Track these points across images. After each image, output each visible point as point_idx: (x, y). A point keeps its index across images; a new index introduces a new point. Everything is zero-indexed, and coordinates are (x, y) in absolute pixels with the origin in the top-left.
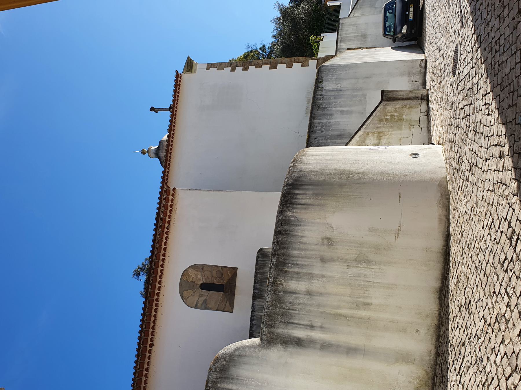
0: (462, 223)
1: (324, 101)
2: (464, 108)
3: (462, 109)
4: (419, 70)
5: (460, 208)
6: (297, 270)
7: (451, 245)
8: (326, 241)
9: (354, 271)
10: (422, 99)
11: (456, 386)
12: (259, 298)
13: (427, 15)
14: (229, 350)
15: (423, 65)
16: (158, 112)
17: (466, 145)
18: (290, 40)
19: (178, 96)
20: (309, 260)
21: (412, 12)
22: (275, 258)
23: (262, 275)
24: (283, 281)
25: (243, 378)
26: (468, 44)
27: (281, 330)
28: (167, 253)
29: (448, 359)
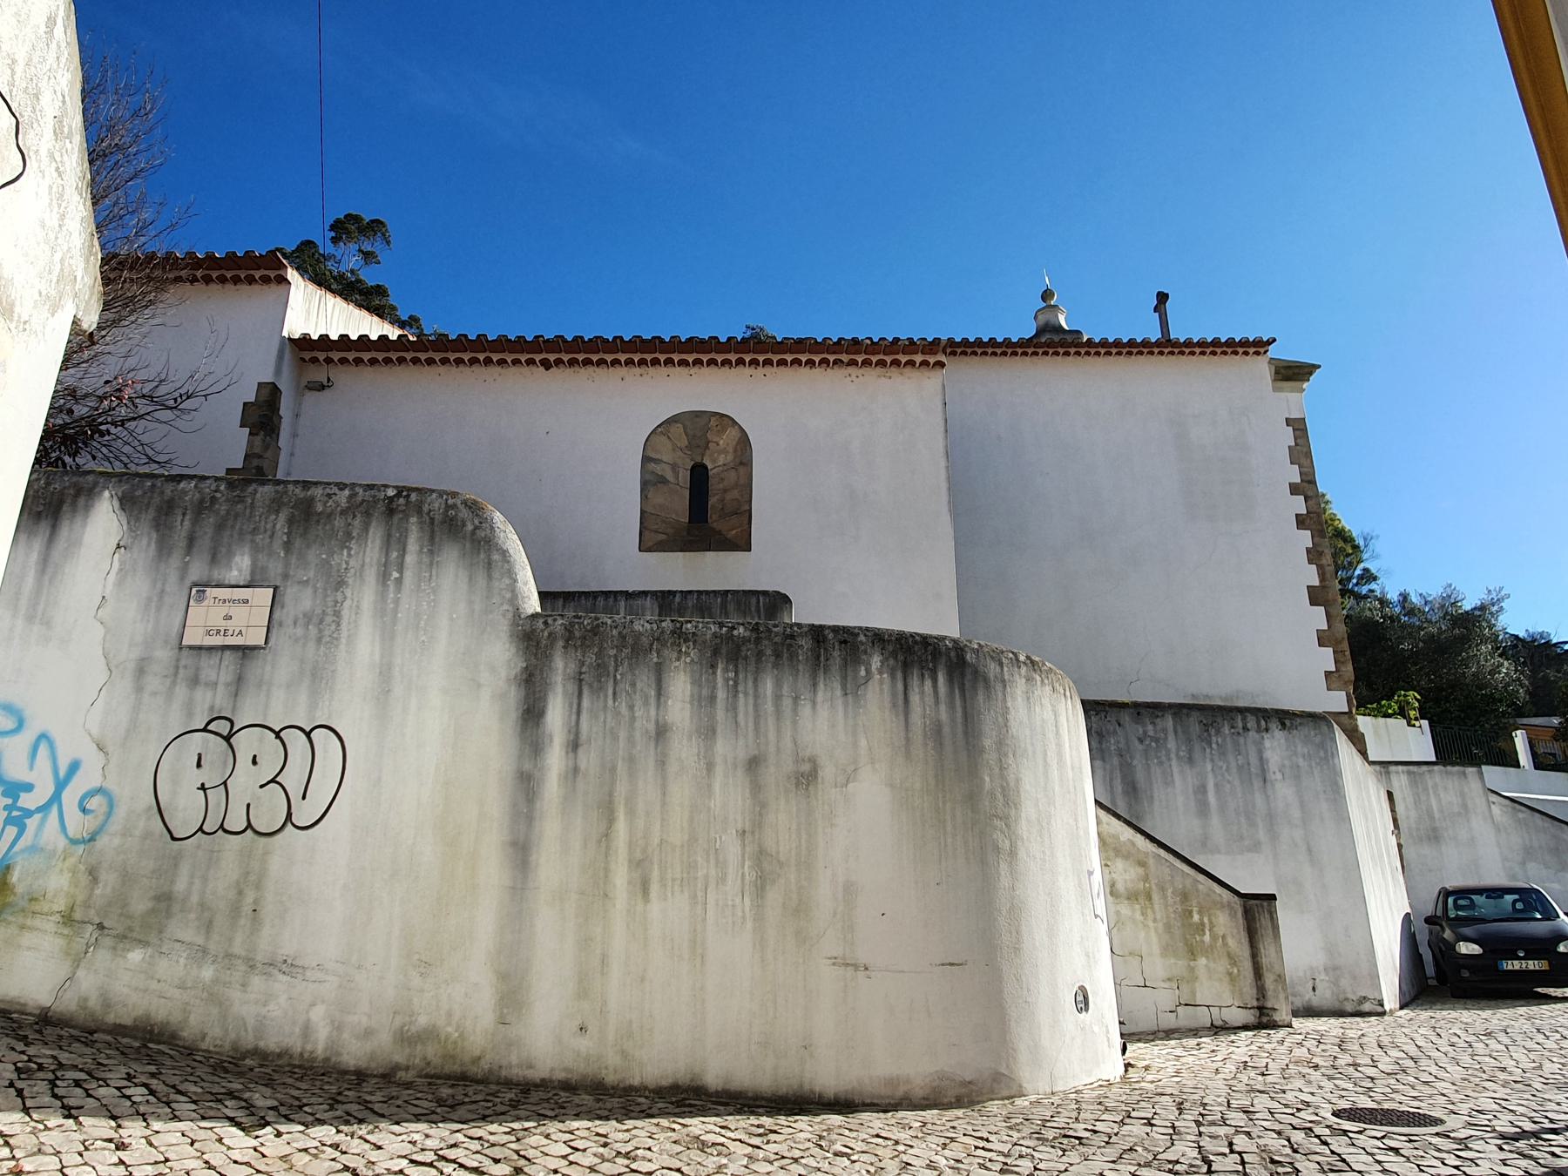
0: (876, 1155)
1: (1228, 739)
2: (1232, 1152)
3: (1231, 1144)
4: (1351, 996)
5: (924, 1146)
6: (721, 694)
7: (818, 1119)
8: (806, 767)
9: (732, 849)
10: (1261, 1009)
11: (408, 1149)
12: (660, 607)
13: (1522, 1010)
14: (502, 535)
15: (1367, 1007)
16: (1157, 314)
17: (1114, 1162)
18: (1401, 640)
19: (1203, 353)
20: (751, 724)
21: (1524, 966)
22: (748, 634)
23: (721, 609)
24: (688, 660)
25: (434, 578)
26: (1446, 1162)
27: (561, 666)
28: (775, 369)
29: (492, 1123)
